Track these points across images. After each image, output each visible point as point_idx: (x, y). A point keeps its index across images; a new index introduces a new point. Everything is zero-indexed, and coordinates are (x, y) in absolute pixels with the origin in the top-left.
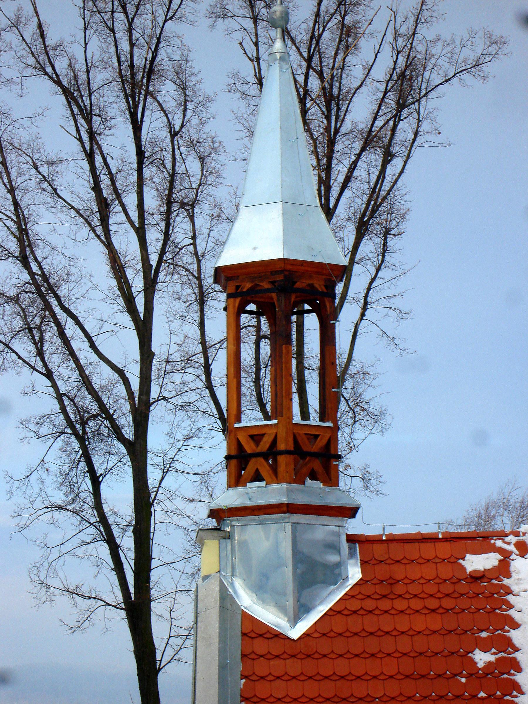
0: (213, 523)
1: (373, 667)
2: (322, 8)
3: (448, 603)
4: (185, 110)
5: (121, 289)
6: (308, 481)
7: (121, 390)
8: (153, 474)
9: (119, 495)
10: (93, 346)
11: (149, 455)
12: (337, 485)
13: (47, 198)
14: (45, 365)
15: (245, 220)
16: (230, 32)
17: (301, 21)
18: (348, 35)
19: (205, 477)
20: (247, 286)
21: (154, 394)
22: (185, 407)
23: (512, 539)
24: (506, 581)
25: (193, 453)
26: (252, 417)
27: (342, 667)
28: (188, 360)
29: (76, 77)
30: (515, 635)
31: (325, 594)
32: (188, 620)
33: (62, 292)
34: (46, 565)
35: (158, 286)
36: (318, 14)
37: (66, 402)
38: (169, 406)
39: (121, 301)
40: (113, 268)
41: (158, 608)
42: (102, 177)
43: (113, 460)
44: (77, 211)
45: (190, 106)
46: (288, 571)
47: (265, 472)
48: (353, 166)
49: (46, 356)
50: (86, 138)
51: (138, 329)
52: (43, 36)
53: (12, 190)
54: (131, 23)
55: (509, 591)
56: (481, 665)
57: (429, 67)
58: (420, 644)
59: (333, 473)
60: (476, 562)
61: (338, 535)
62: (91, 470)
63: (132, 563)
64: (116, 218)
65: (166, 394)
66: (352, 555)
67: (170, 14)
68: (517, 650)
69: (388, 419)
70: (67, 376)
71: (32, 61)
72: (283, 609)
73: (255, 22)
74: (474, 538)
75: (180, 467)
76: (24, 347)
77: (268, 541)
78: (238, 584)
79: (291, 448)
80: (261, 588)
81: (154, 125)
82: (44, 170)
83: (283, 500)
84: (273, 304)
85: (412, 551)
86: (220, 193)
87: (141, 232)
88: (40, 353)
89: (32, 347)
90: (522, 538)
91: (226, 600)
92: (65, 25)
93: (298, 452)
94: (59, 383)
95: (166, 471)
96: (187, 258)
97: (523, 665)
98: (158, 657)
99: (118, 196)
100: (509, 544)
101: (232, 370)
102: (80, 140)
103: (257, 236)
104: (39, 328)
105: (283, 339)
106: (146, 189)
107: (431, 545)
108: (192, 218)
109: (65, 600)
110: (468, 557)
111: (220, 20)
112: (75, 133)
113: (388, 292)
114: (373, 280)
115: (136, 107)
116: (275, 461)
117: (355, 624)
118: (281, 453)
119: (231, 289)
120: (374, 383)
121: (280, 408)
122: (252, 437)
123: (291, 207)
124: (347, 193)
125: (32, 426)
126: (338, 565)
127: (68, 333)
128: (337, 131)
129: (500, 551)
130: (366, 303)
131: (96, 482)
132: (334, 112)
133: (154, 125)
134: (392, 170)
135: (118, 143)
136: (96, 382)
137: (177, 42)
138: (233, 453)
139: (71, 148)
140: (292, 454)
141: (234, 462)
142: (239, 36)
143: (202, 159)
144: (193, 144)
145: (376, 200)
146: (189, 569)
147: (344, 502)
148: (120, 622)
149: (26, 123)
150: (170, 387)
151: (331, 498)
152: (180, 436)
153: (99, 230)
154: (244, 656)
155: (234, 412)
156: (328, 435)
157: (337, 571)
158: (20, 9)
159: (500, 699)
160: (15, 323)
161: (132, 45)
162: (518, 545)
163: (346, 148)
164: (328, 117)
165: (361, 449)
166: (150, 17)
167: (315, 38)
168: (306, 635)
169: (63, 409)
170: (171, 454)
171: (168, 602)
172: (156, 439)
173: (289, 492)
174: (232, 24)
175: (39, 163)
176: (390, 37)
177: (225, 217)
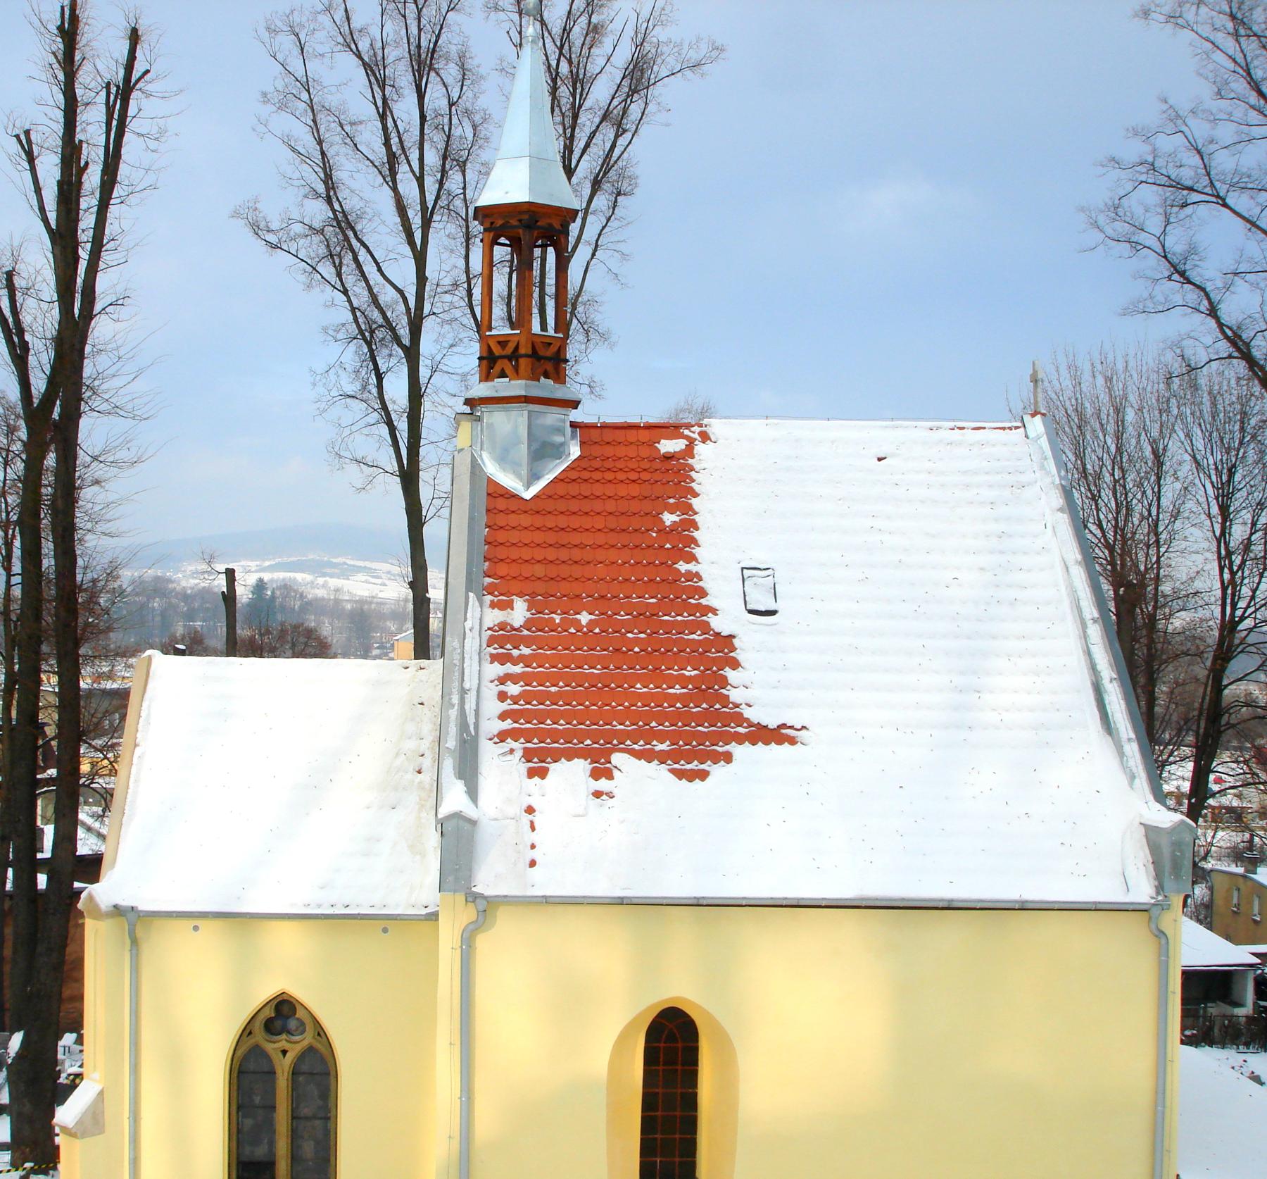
0: (467, 409)
2: (574, 6)
3: (645, 476)
6: (542, 379)
7: (402, 307)
8: (424, 372)
9: (397, 389)
10: (380, 270)
12: (564, 382)
13: (349, 150)
17: (555, 15)
18: (594, 31)
19: (464, 376)
20: (499, 222)
21: (426, 310)
22: (450, 322)
23: (697, 429)
24: (690, 461)
25: (456, 358)
26: (501, 328)
27: (562, 521)
28: (455, 285)
29: (375, 54)
30: (695, 502)
31: (551, 465)
33: (358, 227)
36: (569, 12)
37: (358, 314)
38: (438, 320)
39: (403, 235)
43: (393, 361)
45: (467, 83)
46: (524, 448)
48: (593, 134)
49: (344, 277)
50: (380, 103)
51: (415, 258)
52: (348, 19)
53: (320, 143)
54: (419, 11)
55: (692, 469)
56: (668, 523)
57: (659, 61)
60: (668, 446)
61: (564, 421)
64: (403, 168)
66: (573, 437)
69: (614, 339)
70: (360, 296)
71: (341, 40)
72: (519, 476)
75: (445, 368)
76: (327, 270)
77: (509, 424)
78: (485, 455)
80: (503, 459)
81: (436, 98)
82: (347, 128)
85: (620, 435)
86: (485, 155)
87: (420, 180)
88: (339, 275)
89: (333, 270)
91: (475, 467)
93: (535, 355)
95: (433, 372)
100: (694, 433)
102: (375, 104)
103: (509, 182)
106: (426, 146)
107: (634, 432)
114: (604, 228)
115: (421, 80)
116: (517, 361)
117: (574, 489)
118: (522, 356)
119: (488, 224)
120: (601, 309)
121: (519, 320)
122: (499, 343)
123: (537, 161)
124: (585, 157)
125: (331, 332)
126: (562, 444)
128: (580, 106)
129: (687, 437)
130: (597, 246)
131: (380, 378)
132: (578, 91)
133: (435, 95)
134: (622, 142)
135: (405, 109)
137: (456, 28)
138: (485, 355)
140: (530, 357)
141: (485, 362)
142: (507, 25)
143: (475, 127)
144: (468, 113)
145: (607, 162)
148: (396, 485)
151: (560, 392)
152: (446, 344)
154: (488, 511)
155: (486, 323)
159: (681, 549)
161: (420, 30)
163: (587, 121)
167: (566, 31)
168: (536, 497)
169: (356, 320)
170: (438, 358)
171: (433, 471)
177: (486, 172)
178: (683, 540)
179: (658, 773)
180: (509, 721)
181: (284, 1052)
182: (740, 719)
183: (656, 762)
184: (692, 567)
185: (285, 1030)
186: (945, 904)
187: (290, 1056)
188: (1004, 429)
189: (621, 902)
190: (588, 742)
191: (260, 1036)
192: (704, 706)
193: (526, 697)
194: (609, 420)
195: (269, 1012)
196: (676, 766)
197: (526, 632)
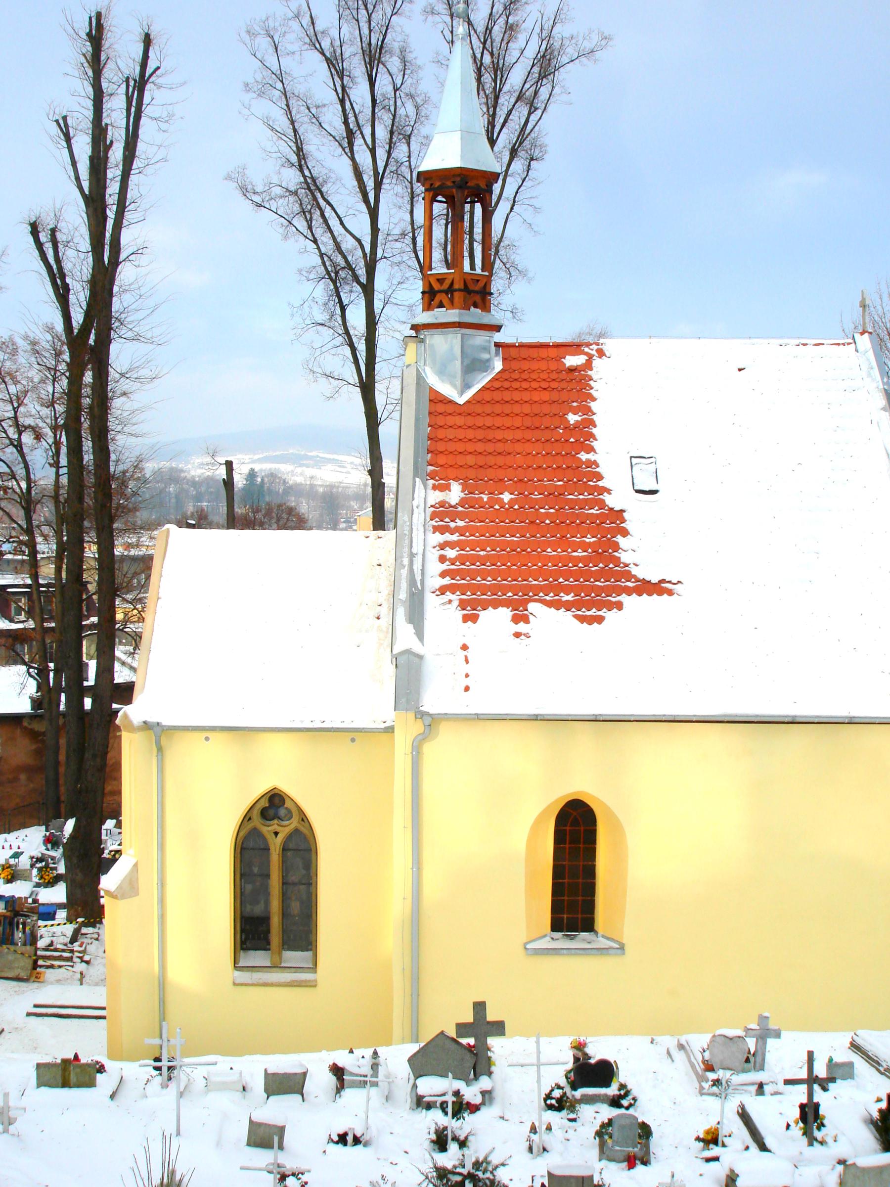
0: (413, 333)
1: (508, 422)
2: (495, 10)
3: (554, 385)
4: (404, 75)
5: (360, 187)
6: (472, 309)
7: (359, 253)
8: (378, 305)
9: (357, 318)
10: (342, 223)
11: (376, 293)
13: (315, 128)
14: (313, 235)
15: (437, 142)
16: (435, 24)
17: (480, 18)
18: (511, 29)
19: (411, 307)
20: (437, 184)
21: (379, 255)
23: (595, 347)
24: (589, 373)
26: (439, 268)
27: (489, 421)
28: (403, 235)
29: (335, 51)
30: (593, 405)
32: (397, 395)
33: (324, 189)
34: (313, 359)
35: (383, 186)
36: (491, 14)
37: (326, 259)
39: (360, 195)
40: (355, 174)
41: (379, 387)
42: (350, 115)
44: (334, 137)
45: (407, 72)
46: (458, 364)
47: (446, 302)
48: (509, 113)
50: (339, 90)
51: (370, 213)
52: (313, 23)
55: (591, 379)
56: (572, 422)
58: (536, 409)
59: (487, 304)
60: (572, 361)
61: (490, 342)
62: (340, 301)
63: (364, 359)
65: (386, 255)
66: (497, 354)
67: (395, 11)
68: (594, 414)
72: (455, 386)
73: (452, 18)
74: (571, 346)
75: (394, 301)
77: (446, 344)
78: (428, 369)
79: (462, 287)
80: (441, 372)
81: (383, 84)
82: (314, 111)
83: (457, 320)
84: (454, 197)
85: (534, 353)
86: (424, 130)
88: (310, 228)
89: (305, 223)
90: (600, 347)
92: (327, 17)
93: (466, 289)
94: (321, 246)
96: (405, 170)
97: (597, 423)
98: (379, 416)
99: (360, 129)
101: (427, 238)
102: (336, 91)
103: (444, 152)
104: (310, 212)
105: (456, 219)
108: (409, 145)
109: (323, 380)
110: (567, 357)
111: (430, 17)
112: (332, 87)
113: (529, 195)
114: (520, 187)
115: (372, 69)
116: (452, 295)
118: (456, 290)
119: (428, 186)
121: (453, 262)
123: (467, 134)
124: (504, 130)
125: (304, 273)
126: (488, 360)
127: (327, 215)
128: (500, 90)
129: (586, 354)
130: (514, 201)
131: (343, 309)
132: (499, 77)
134: (534, 118)
135: (360, 94)
136: (344, 247)
137: (398, 29)
138: (427, 290)
139: (332, 97)
140: (463, 292)
141: (427, 295)
142: (441, 26)
146: (400, 364)
147: (493, 322)
148: (356, 394)
149: (302, 80)
150: (389, 250)
151: (486, 319)
152: (395, 282)
153: (347, 150)
154: (430, 413)
156: (485, 281)
157: (487, 364)
158: (300, 6)
160: (295, 208)
161: (370, 31)
162: (597, 351)
163: (506, 102)
164: (495, 81)
165: (506, 293)
166: (381, 13)
167: (488, 30)
168: (468, 402)
169: (324, 263)
170: (389, 293)
172: (380, 283)
173: (460, 315)
174: (437, 18)
175: (310, 106)
176: (537, 30)
178: (584, 434)
179: (565, 617)
180: (448, 578)
181: (276, 834)
182: (629, 576)
183: (563, 610)
184: (591, 456)
185: (276, 817)
186: (790, 720)
187: (281, 836)
188: (839, 344)
189: (535, 718)
190: (510, 594)
191: (257, 821)
192: (601, 565)
193: (461, 559)
194: (525, 340)
195: (265, 803)
196: (579, 613)
197: (460, 509)
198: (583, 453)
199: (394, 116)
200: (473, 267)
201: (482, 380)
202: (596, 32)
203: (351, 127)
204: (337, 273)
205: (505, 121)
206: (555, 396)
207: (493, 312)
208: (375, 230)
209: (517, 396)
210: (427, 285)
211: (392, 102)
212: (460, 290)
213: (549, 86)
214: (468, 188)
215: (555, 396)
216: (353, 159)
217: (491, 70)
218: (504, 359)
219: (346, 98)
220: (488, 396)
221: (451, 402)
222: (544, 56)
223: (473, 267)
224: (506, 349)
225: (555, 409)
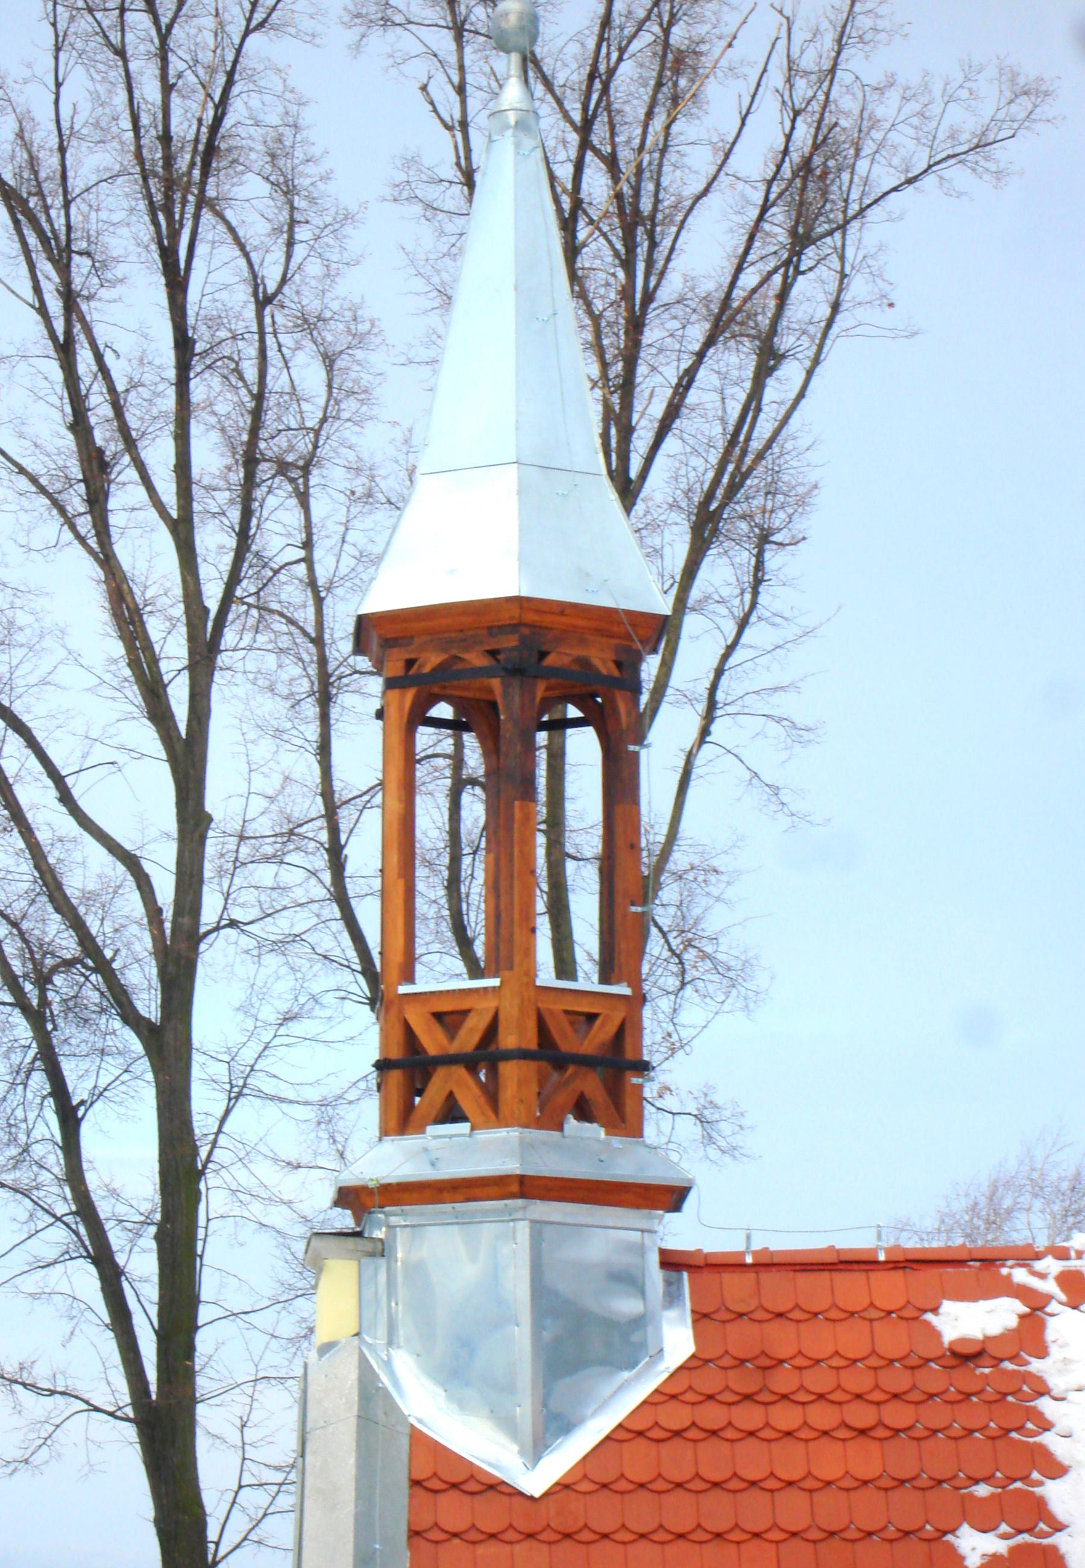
0: (345, 1219)
3: (897, 1415)
4: (290, 244)
5: (134, 663)
6: (572, 1124)
7: (132, 903)
8: (205, 1103)
9: (123, 1153)
10: (66, 798)
16: (398, 61)
20: (432, 660)
21: (209, 915)
23: (1051, 1265)
24: (1036, 1365)
26: (440, 971)
29: (33, 162)
30: (1056, 1494)
32: (285, 1448)
35: (222, 659)
36: (606, 22)
39: (134, 692)
41: (210, 1419)
42: (94, 400)
44: (34, 480)
45: (302, 233)
46: (521, 1336)
47: (469, 1098)
50: (55, 306)
51: (174, 760)
55: (1042, 1390)
58: (831, 1510)
59: (629, 1104)
60: (963, 1320)
61: (641, 1250)
62: (59, 1090)
63: (153, 1311)
65: (237, 914)
66: (671, 1298)
67: (258, 17)
72: (508, 1425)
73: (459, 38)
77: (478, 1261)
78: (404, 1362)
79: (531, 1042)
80: (455, 1373)
83: (511, 1166)
84: (493, 705)
85: (814, 1290)
86: (366, 440)
90: (1073, 1264)
93: (547, 1051)
98: (212, 1534)
99: (130, 444)
101: (394, 858)
102: (42, 310)
108: (303, 499)
110: (948, 1307)
111: (376, 33)
112: (29, 294)
114: (730, 649)
116: (493, 1072)
118: (508, 1056)
119: (395, 668)
123: (538, 470)
124: (671, 444)
126: (639, 1322)
128: (649, 297)
129: (1022, 1293)
130: (712, 704)
132: (642, 251)
135: (131, 318)
136: (74, 884)
138: (395, 1054)
140: (531, 1056)
141: (396, 1076)
142: (419, 69)
147: (654, 1174)
148: (122, 1450)
150: (248, 896)
151: (624, 1162)
152: (269, 1013)
153: (85, 525)
154: (414, 1534)
157: (635, 1337)
161: (167, 89)
164: (628, 264)
165: (698, 1050)
167: (599, 77)
168: (563, 1487)
170: (247, 1056)
172: (213, 1020)
173: (525, 1147)
174: (405, 41)
176: (776, 77)
198: (965, 1530)
199: (259, 398)
200: (565, 966)
201: (618, 1401)
202: (992, 72)
203: (99, 441)
204: (43, 980)
205: (673, 412)
206: (902, 1459)
207: (649, 1130)
208: (193, 820)
209: (752, 1460)
210: (398, 1033)
211: (251, 351)
212: (522, 1055)
213: (827, 274)
214: (552, 672)
215: (902, 1459)
216: (107, 560)
217: (613, 227)
218: (700, 1317)
219: (81, 338)
220: (639, 1463)
221: (495, 1487)
222: (806, 164)
223: (565, 966)
224: (707, 1277)
225: (906, 1508)
